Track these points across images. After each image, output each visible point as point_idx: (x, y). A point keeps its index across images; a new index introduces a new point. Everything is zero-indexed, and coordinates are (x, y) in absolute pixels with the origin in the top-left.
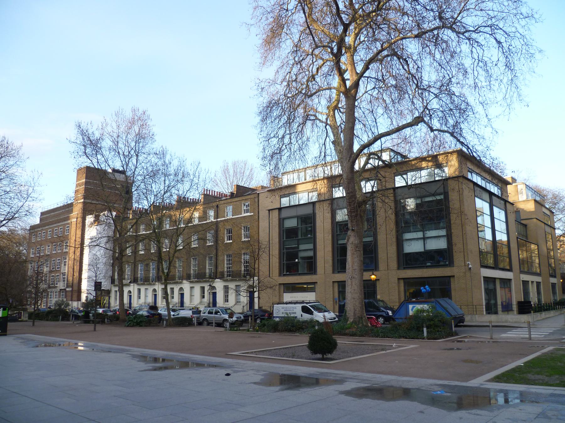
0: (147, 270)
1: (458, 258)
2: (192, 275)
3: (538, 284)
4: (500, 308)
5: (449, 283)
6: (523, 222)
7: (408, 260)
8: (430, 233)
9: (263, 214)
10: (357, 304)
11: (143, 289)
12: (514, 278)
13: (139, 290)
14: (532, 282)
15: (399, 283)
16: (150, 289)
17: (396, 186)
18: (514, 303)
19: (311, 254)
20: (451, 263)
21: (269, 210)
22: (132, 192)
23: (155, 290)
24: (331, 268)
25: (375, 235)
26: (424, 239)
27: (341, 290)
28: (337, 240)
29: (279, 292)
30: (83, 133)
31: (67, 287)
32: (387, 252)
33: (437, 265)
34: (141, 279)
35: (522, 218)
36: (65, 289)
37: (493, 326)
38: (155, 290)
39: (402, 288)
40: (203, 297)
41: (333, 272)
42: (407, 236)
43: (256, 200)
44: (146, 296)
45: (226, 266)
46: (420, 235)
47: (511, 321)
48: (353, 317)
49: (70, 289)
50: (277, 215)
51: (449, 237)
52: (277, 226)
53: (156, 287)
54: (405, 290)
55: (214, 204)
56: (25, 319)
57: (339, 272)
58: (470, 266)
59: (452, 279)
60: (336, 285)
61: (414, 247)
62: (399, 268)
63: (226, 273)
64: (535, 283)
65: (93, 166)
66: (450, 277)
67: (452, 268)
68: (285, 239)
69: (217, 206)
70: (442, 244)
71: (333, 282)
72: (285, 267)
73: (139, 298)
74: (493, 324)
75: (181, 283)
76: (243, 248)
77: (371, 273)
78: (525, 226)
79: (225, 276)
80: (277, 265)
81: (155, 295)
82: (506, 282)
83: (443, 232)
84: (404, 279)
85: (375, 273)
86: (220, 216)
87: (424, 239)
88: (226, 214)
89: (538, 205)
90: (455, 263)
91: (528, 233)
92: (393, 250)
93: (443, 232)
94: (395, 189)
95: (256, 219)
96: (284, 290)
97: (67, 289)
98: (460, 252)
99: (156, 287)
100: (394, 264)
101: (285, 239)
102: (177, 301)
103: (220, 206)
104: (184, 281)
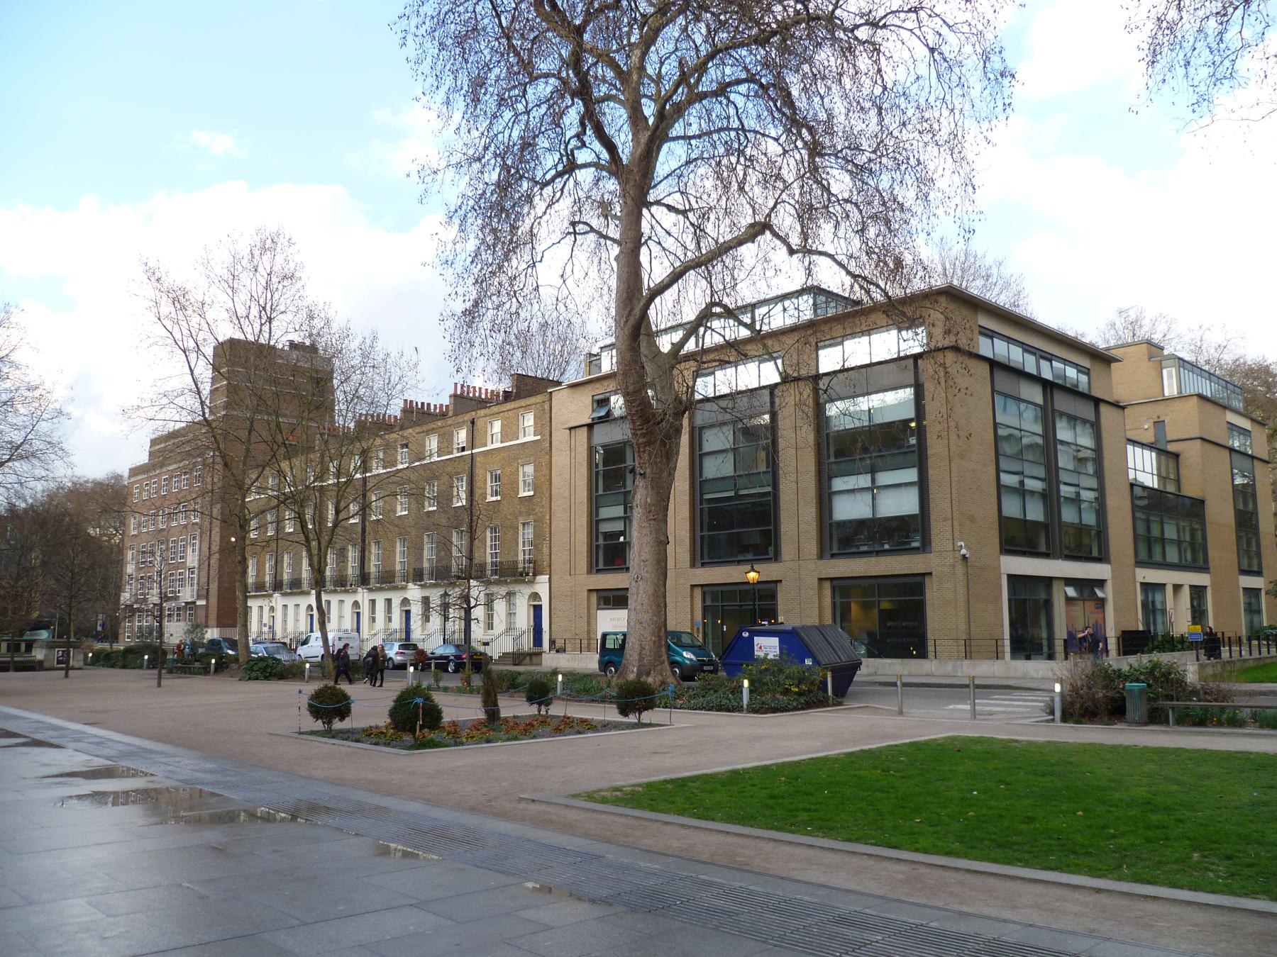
0: (388, 555)
1: (940, 532)
2: (426, 572)
3: (1198, 593)
4: (1059, 647)
5: (773, 596)
6: (1171, 448)
7: (842, 538)
8: (885, 478)
9: (560, 436)
10: (647, 634)
11: (380, 599)
12: (1114, 578)
13: (373, 602)
14: (1177, 588)
15: (820, 588)
16: (349, 600)
17: (821, 371)
18: (1112, 634)
19: (619, 526)
20: (925, 546)
21: (570, 429)
22: (332, 391)
23: (356, 604)
24: (687, 557)
25: (775, 484)
26: (873, 489)
27: (708, 603)
28: (701, 495)
29: (589, 609)
30: (154, 276)
31: (199, 597)
32: (797, 521)
33: (902, 548)
34: (495, 572)
35: (1169, 438)
36: (194, 603)
37: (905, 685)
38: (356, 604)
39: (828, 601)
40: (390, 620)
41: (693, 565)
42: (839, 484)
43: (547, 406)
44: (341, 617)
45: (488, 551)
46: (864, 481)
47: (1035, 675)
48: (637, 664)
49: (203, 602)
50: (585, 440)
51: (923, 485)
52: (585, 464)
53: (359, 597)
54: (834, 604)
55: (468, 417)
56: (77, 665)
57: (703, 565)
58: (964, 551)
59: (927, 579)
60: (698, 592)
61: (848, 509)
62: (821, 556)
63: (489, 567)
64: (1186, 592)
65: (242, 337)
66: (924, 575)
67: (928, 555)
68: (601, 492)
69: (473, 422)
70: (901, 504)
71: (693, 586)
72: (601, 553)
73: (374, 620)
74: (906, 680)
75: (404, 588)
76: (521, 513)
77: (749, 567)
78: (1176, 456)
79: (489, 573)
80: (585, 548)
81: (408, 612)
82: (1087, 587)
83: (911, 475)
84: (831, 579)
85: (756, 567)
86: (477, 442)
87: (873, 489)
88: (521, 431)
89: (1210, 407)
90: (933, 544)
91: (1182, 471)
92: (809, 512)
93: (911, 475)
94: (817, 377)
95: (541, 451)
96: (598, 604)
97: (199, 603)
98: (945, 519)
99: (359, 597)
100: (811, 547)
101: (601, 492)
102: (525, 627)
103: (479, 423)
104: (411, 585)
